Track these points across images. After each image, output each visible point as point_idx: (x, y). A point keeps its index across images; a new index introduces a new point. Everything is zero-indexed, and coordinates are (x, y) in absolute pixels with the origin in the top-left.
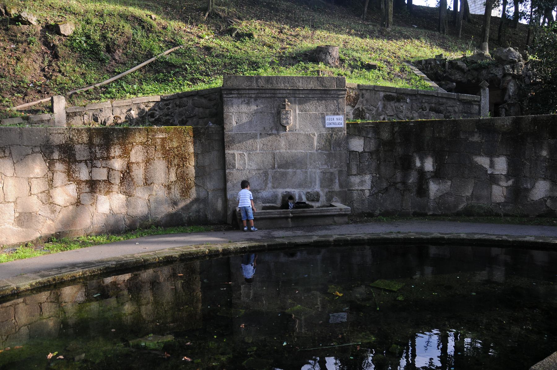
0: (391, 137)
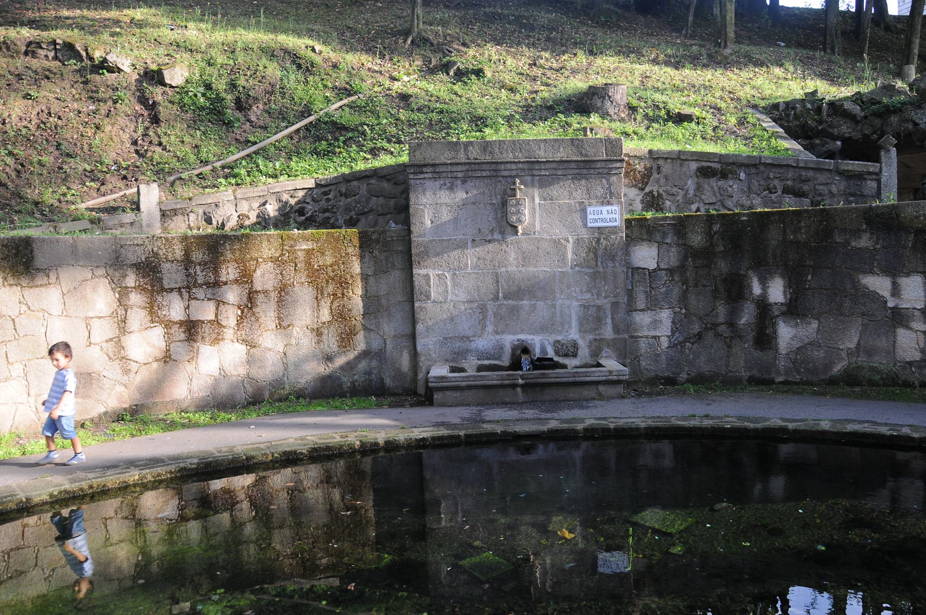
0: (706, 241)
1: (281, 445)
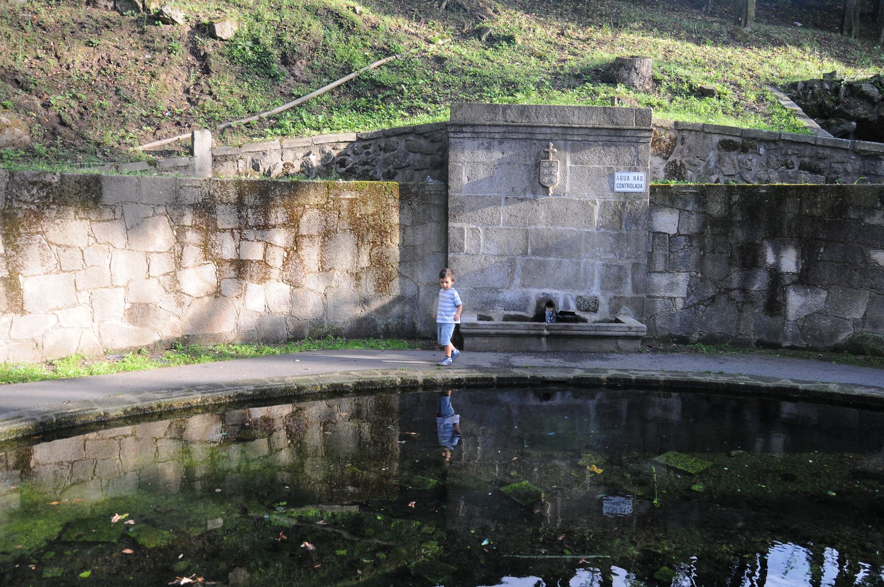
1: (329, 378)
